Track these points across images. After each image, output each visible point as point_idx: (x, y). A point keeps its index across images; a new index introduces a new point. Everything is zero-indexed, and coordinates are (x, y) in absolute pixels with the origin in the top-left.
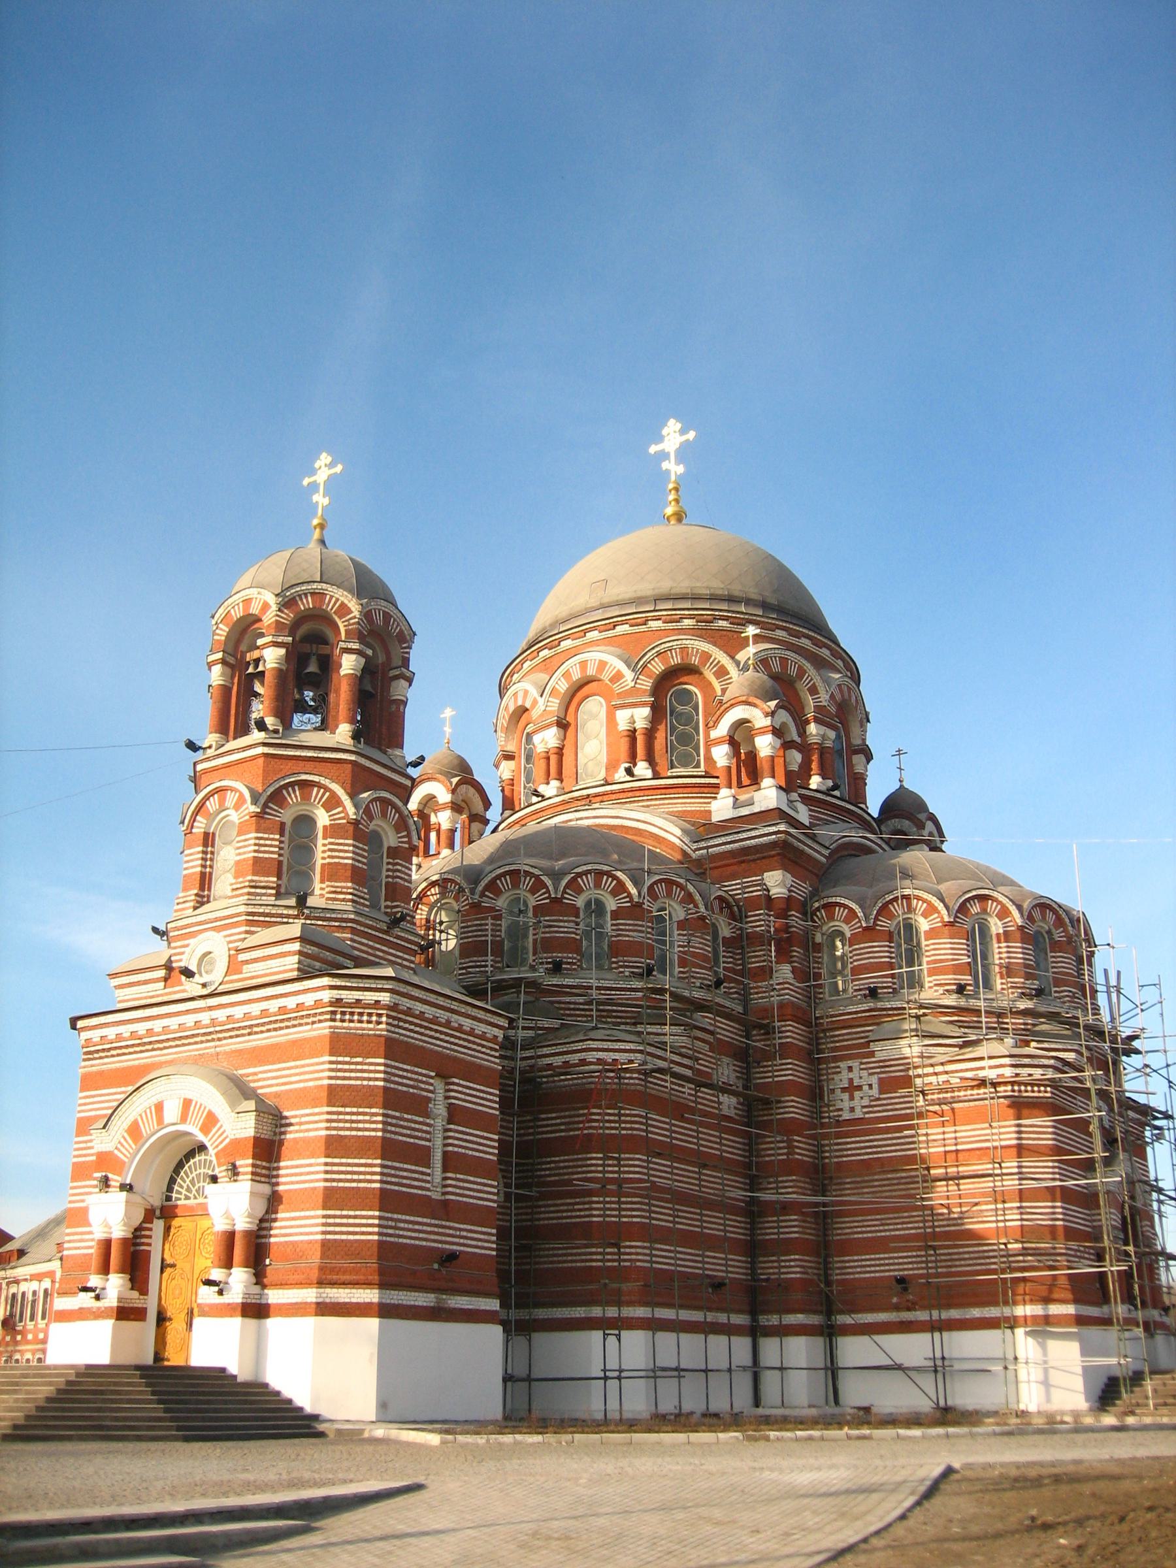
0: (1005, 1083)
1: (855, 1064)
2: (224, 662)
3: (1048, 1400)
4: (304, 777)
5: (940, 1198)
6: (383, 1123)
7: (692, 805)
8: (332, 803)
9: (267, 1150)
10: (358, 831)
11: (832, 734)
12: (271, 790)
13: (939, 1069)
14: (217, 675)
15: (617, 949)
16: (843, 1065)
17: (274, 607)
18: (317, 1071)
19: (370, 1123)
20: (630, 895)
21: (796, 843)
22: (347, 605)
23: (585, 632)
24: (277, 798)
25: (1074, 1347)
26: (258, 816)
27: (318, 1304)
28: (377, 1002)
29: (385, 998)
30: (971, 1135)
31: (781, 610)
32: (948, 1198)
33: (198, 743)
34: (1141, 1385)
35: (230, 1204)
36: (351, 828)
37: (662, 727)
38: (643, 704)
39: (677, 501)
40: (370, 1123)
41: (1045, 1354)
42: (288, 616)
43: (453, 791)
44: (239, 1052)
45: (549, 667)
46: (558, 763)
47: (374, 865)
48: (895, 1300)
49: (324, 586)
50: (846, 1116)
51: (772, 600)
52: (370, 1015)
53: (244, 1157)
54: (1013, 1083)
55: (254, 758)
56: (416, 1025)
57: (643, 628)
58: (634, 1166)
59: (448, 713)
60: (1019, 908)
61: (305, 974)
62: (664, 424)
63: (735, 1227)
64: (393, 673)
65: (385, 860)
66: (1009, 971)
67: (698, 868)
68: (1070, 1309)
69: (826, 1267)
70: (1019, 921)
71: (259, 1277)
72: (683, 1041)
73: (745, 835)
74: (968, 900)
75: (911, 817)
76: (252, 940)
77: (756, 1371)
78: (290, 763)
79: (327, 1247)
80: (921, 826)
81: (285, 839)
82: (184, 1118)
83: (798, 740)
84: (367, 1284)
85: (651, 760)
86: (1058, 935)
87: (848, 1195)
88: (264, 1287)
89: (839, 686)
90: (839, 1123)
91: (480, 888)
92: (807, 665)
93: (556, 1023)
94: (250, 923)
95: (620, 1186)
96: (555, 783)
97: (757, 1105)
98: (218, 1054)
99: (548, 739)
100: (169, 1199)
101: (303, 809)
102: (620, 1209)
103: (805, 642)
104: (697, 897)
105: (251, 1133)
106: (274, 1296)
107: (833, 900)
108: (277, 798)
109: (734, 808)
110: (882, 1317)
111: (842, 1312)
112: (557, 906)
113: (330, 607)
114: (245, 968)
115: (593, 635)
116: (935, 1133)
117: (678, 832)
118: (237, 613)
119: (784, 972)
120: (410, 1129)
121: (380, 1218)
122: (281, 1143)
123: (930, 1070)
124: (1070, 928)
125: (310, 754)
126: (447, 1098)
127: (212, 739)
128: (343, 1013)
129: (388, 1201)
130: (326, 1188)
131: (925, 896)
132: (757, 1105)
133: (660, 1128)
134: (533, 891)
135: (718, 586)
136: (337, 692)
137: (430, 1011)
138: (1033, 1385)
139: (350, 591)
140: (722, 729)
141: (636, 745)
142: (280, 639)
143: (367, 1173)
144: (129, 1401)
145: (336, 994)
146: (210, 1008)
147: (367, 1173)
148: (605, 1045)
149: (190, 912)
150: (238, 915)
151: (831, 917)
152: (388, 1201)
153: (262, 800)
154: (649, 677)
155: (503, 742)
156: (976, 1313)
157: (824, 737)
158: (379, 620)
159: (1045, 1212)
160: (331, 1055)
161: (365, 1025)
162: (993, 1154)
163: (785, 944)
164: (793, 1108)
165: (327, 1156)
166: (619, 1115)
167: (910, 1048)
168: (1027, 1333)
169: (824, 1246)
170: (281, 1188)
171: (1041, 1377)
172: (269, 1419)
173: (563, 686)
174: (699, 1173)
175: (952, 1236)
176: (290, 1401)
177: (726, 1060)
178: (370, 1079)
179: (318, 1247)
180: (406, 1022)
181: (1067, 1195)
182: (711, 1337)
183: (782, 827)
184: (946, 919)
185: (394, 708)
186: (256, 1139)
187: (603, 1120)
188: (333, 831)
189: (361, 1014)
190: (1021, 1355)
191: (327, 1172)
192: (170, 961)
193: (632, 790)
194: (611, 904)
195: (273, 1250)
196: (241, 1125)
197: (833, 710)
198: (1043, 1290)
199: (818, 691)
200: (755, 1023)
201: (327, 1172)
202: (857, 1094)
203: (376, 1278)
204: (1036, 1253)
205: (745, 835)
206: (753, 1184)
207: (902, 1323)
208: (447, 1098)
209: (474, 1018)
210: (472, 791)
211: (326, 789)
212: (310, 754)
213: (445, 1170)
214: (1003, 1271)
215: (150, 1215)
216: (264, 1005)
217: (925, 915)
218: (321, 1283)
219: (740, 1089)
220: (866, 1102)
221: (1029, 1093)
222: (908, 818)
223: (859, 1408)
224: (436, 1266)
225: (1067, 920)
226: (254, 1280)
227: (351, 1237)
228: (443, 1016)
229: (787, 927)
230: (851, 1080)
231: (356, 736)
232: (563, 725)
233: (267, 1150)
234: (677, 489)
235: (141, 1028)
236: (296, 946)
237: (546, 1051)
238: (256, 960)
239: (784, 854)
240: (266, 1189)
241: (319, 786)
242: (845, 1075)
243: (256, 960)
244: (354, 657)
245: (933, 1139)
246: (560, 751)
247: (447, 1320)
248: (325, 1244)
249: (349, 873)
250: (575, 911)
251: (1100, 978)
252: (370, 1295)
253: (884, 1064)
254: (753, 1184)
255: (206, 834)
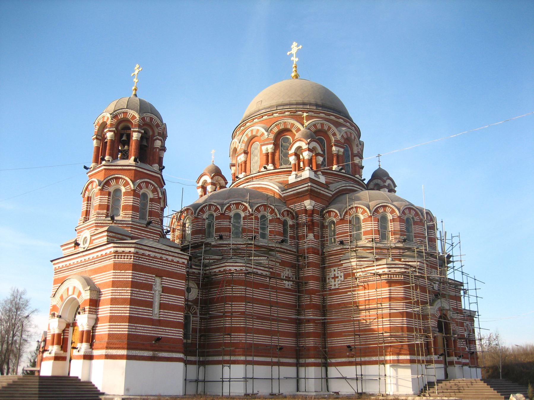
0: (386, 274)
1: (336, 269)
2: (97, 138)
3: (398, 390)
4: (116, 176)
5: (363, 316)
6: (131, 293)
7: (282, 178)
8: (126, 184)
9: (94, 303)
10: (134, 193)
11: (342, 150)
12: (105, 181)
13: (363, 270)
14: (95, 143)
15: (244, 230)
16: (332, 269)
17: (110, 118)
18: (108, 276)
19: (126, 293)
20: (249, 211)
21: (316, 190)
22: (134, 115)
23: (253, 120)
24: (107, 183)
25: (409, 371)
26: (100, 190)
27: (106, 355)
28: (130, 251)
29: (132, 250)
30: (372, 293)
31: (323, 106)
32: (366, 316)
33: (88, 166)
34: (433, 388)
35: (83, 322)
36: (132, 192)
37: (278, 151)
38: (270, 144)
39: (296, 71)
40: (126, 293)
41: (397, 374)
42: (115, 120)
43: (212, 178)
44: (91, 270)
45: (243, 132)
46: (245, 166)
47: (145, 205)
48: (348, 354)
49: (128, 110)
50: (333, 287)
51: (320, 103)
52: (128, 256)
53: (87, 306)
54: (388, 275)
55: (102, 170)
56: (147, 259)
57: (272, 117)
58: (240, 307)
59: (213, 151)
60: (399, 209)
61: (109, 243)
62: (292, 44)
63: (289, 328)
64: (155, 138)
65: (149, 202)
66: (394, 233)
67: (285, 200)
68: (408, 357)
69: (325, 341)
70: (398, 214)
71: (91, 346)
72: (266, 262)
73: (297, 188)
74: (379, 207)
75: (380, 179)
76: (97, 232)
77: (298, 379)
78: (113, 171)
79: (110, 336)
80: (385, 182)
81: (111, 197)
82: (73, 293)
83: (322, 153)
84: (123, 348)
85: (273, 163)
86: (416, 219)
87: (333, 316)
88: (93, 349)
89: (346, 132)
90: (330, 290)
91: (198, 211)
92: (332, 126)
93: (221, 257)
94: (96, 226)
95: (232, 314)
96: (244, 174)
97: (299, 286)
98: (86, 271)
99: (242, 158)
100: (75, 320)
101: (116, 187)
102: (231, 322)
103: (332, 118)
104: (276, 211)
105: (88, 297)
106: (96, 352)
107: (330, 209)
108: (107, 183)
109: (296, 178)
110: (343, 360)
111: (330, 358)
112: (223, 216)
113: (129, 117)
114: (94, 242)
115: (256, 120)
116: (361, 292)
117: (278, 188)
118: (101, 122)
119: (311, 236)
120: (143, 295)
121: (129, 326)
122: (100, 300)
123: (360, 270)
124: (421, 216)
125: (120, 168)
126: (162, 284)
127: (92, 165)
128: (118, 256)
129: (131, 320)
130: (110, 316)
131: (362, 206)
132: (299, 286)
133: (251, 292)
134: (215, 211)
135: (299, 100)
136: (132, 146)
137: (152, 254)
138: (392, 385)
139: (137, 112)
140: (292, 151)
141: (270, 158)
142: (111, 129)
143: (125, 310)
144: (29, 388)
145: (115, 249)
146: (84, 256)
147: (125, 310)
148: (232, 264)
149: (82, 224)
150: (93, 224)
151: (330, 216)
152: (131, 320)
153: (102, 185)
154: (273, 133)
155: (230, 161)
156: (374, 358)
157: (338, 151)
158: (148, 120)
159: (399, 322)
160: (114, 270)
161: (126, 260)
162: (380, 301)
163: (311, 226)
164: (312, 285)
165: (111, 305)
166: (232, 289)
167: (354, 262)
168: (390, 366)
169: (324, 333)
170: (99, 316)
171: (395, 382)
172: (79, 394)
173: (246, 139)
174: (271, 308)
175: (365, 331)
176: (97, 388)
177: (287, 268)
178: (127, 278)
179: (107, 336)
180: (142, 258)
181: (408, 315)
182: (248, 366)
183: (309, 184)
184: (370, 215)
185: (155, 150)
186: (90, 299)
187: (228, 291)
188: (126, 194)
189: (125, 256)
190: (388, 374)
191: (111, 310)
192: (76, 240)
193: (266, 174)
194: (243, 215)
195: (96, 337)
196: (86, 295)
197: (343, 141)
198: (397, 350)
199: (337, 134)
200: (299, 255)
201: (111, 310)
202: (337, 279)
203: (126, 346)
204: (395, 336)
205: (297, 188)
206: (299, 313)
207: (349, 362)
208: (162, 284)
209: (173, 256)
210: (220, 178)
211: (124, 179)
212: (120, 168)
213: (160, 309)
214: (381, 343)
215: (68, 325)
216: (97, 254)
217: (362, 214)
218: (107, 348)
219: (294, 279)
220: (339, 282)
221: (395, 278)
222: (380, 179)
223: (335, 393)
224: (154, 342)
225: (420, 213)
226: (89, 347)
227: (118, 332)
228: (159, 256)
229: (312, 220)
230: (335, 275)
231: (135, 160)
232: (246, 153)
233: (94, 303)
234: (296, 67)
235: (68, 263)
236: (106, 234)
237: (214, 267)
238: (96, 239)
239: (312, 194)
240: (95, 316)
241: (122, 178)
242: (333, 273)
243: (96, 239)
244: (137, 133)
245: (361, 295)
246: (245, 162)
247: (157, 361)
248: (109, 335)
249: (131, 208)
250: (230, 218)
251: (438, 236)
252: (124, 352)
253: (346, 268)
254: (299, 313)
255: (88, 197)
